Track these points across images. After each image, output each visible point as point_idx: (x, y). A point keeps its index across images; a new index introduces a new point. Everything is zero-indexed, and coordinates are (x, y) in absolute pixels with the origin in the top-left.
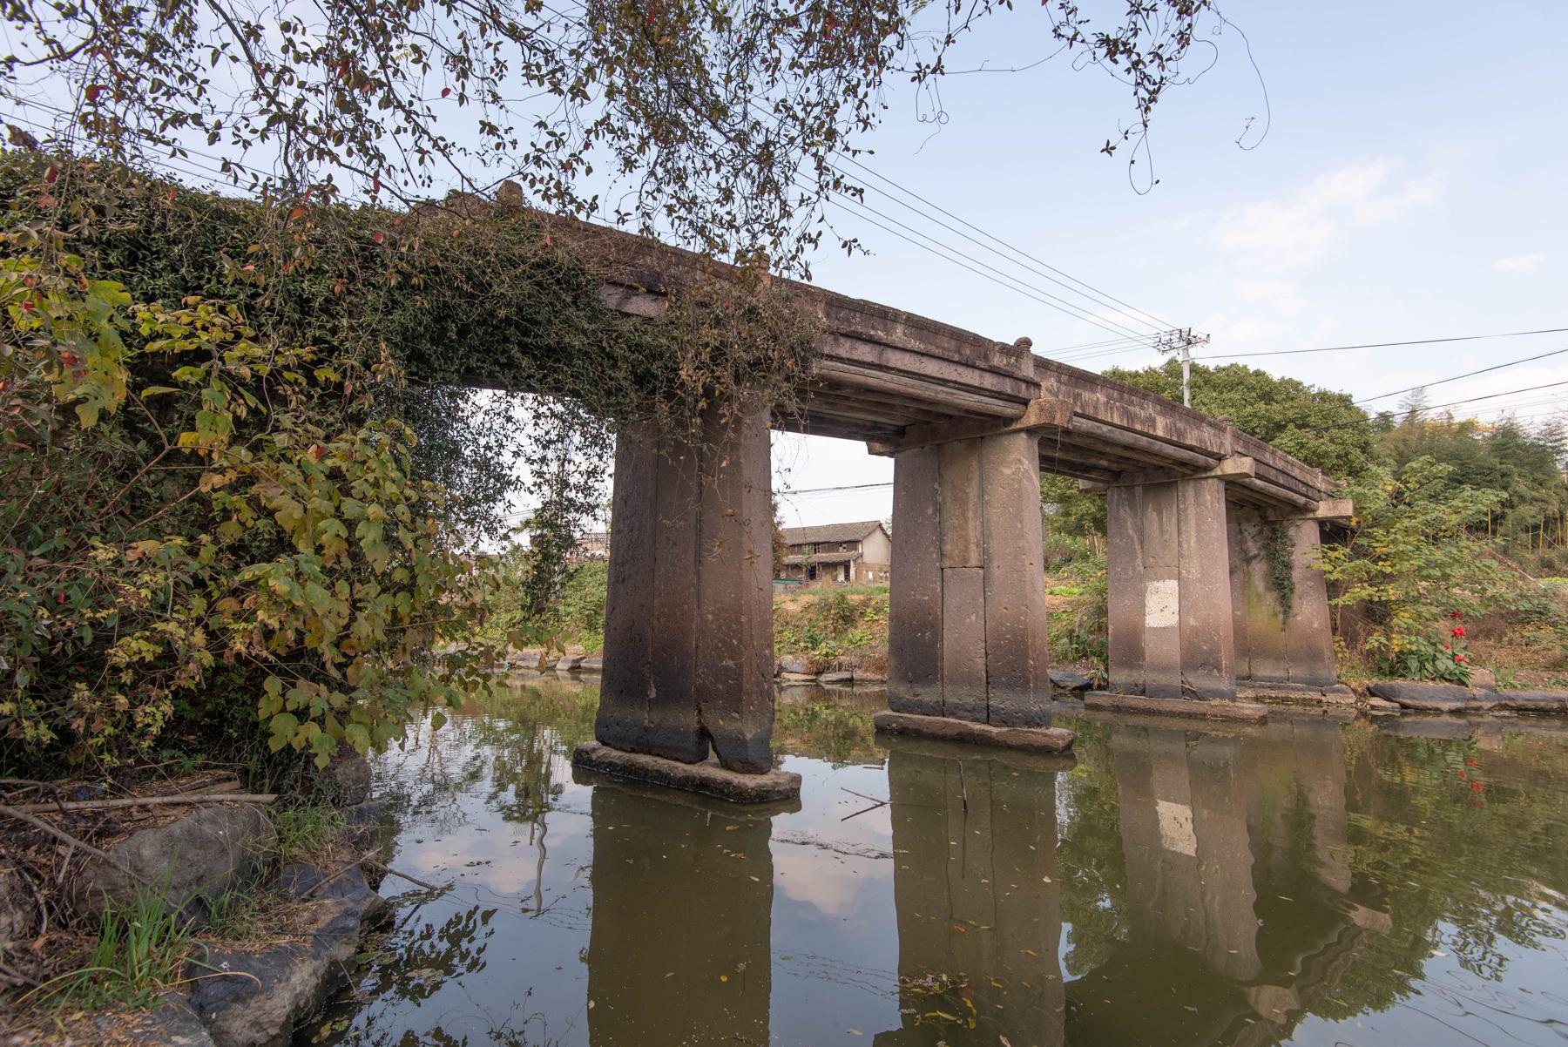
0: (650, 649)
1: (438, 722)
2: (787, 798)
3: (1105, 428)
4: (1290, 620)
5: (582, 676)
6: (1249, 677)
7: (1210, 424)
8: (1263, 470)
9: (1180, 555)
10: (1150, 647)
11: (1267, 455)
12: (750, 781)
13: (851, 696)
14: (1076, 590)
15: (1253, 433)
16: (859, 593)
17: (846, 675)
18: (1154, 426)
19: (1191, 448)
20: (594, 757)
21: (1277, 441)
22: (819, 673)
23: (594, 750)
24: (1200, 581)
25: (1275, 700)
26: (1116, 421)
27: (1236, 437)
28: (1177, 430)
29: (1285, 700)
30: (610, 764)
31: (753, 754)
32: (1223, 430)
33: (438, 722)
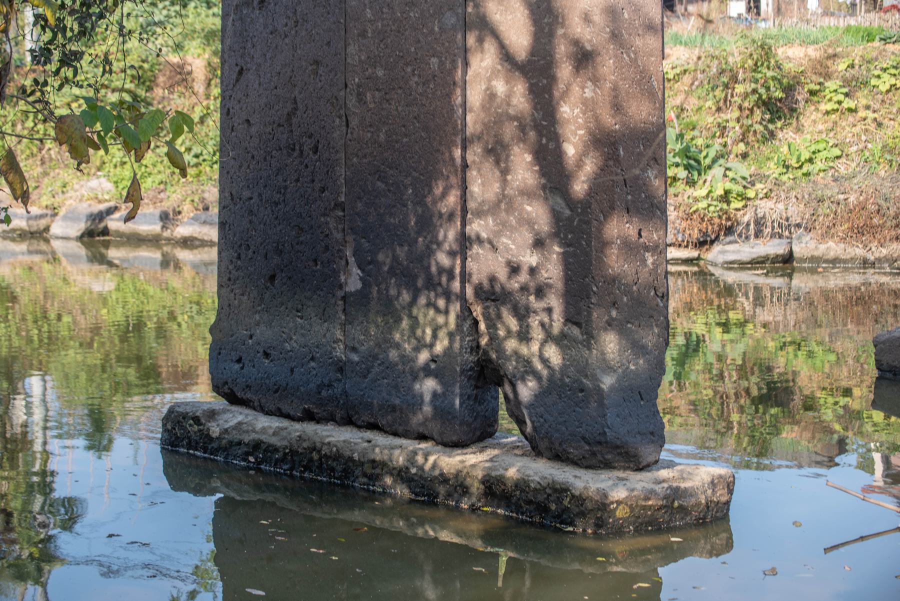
0: (341, 172)
1: (56, 107)
2: (715, 519)
5: (113, 254)
12: (619, 489)
13: (786, 298)
16: (806, 41)
17: (775, 248)
20: (215, 430)
22: (704, 243)
23: (212, 414)
30: (257, 446)
31: (618, 427)
33: (56, 107)
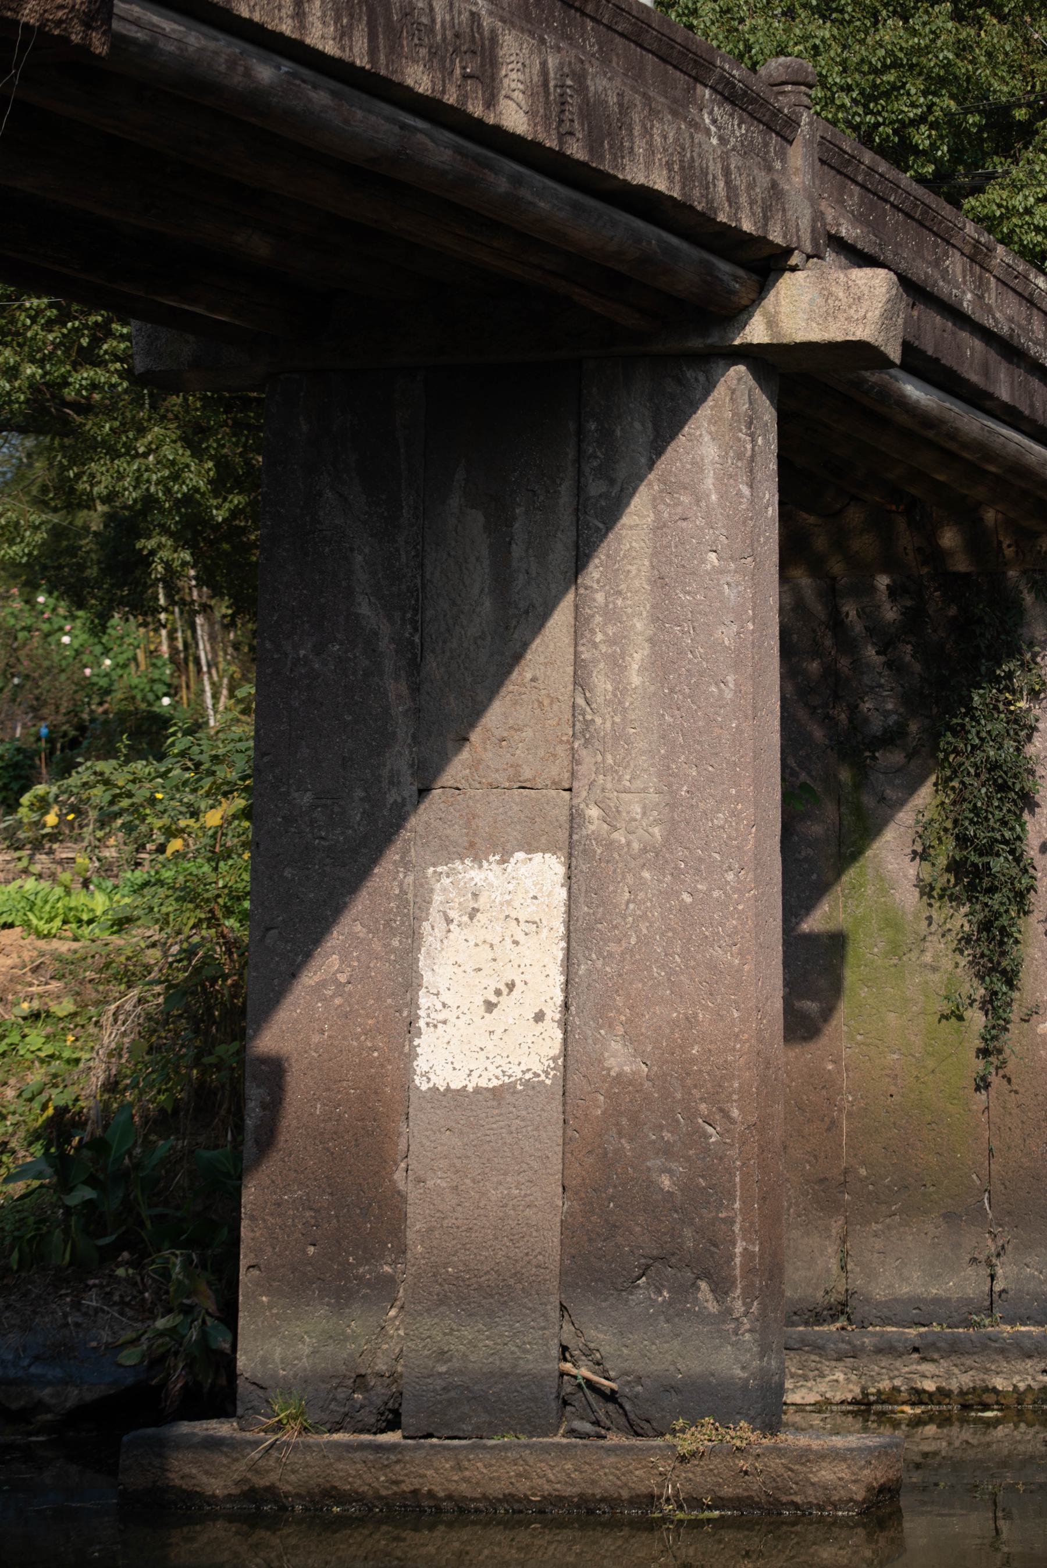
3: (266, 72)
4: (1013, 1039)
6: (839, 1310)
7: (732, 96)
8: (936, 334)
9: (581, 730)
10: (430, 1183)
11: (955, 263)
14: (99, 903)
15: (900, 152)
18: (487, 78)
19: (643, 202)
21: (993, 197)
24: (655, 856)
25: (939, 1408)
26: (321, 36)
27: (833, 162)
28: (591, 111)
29: (974, 1401)
32: (782, 128)
